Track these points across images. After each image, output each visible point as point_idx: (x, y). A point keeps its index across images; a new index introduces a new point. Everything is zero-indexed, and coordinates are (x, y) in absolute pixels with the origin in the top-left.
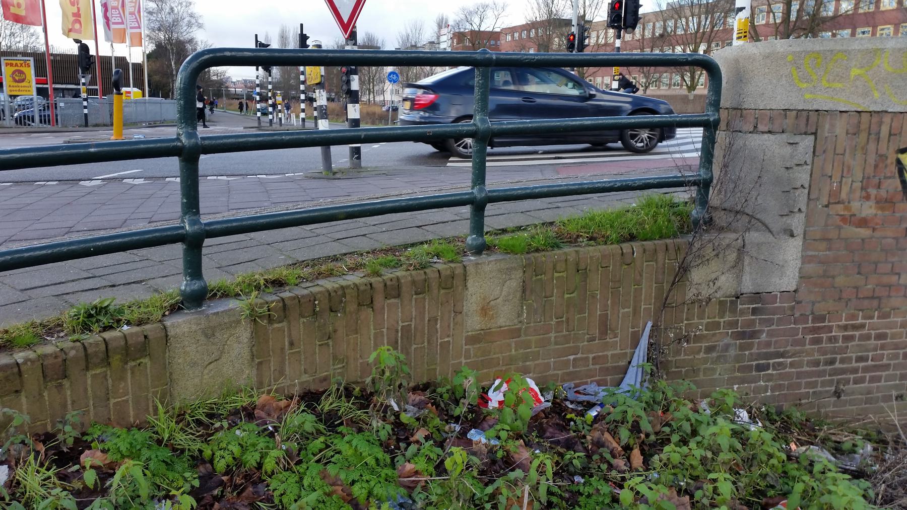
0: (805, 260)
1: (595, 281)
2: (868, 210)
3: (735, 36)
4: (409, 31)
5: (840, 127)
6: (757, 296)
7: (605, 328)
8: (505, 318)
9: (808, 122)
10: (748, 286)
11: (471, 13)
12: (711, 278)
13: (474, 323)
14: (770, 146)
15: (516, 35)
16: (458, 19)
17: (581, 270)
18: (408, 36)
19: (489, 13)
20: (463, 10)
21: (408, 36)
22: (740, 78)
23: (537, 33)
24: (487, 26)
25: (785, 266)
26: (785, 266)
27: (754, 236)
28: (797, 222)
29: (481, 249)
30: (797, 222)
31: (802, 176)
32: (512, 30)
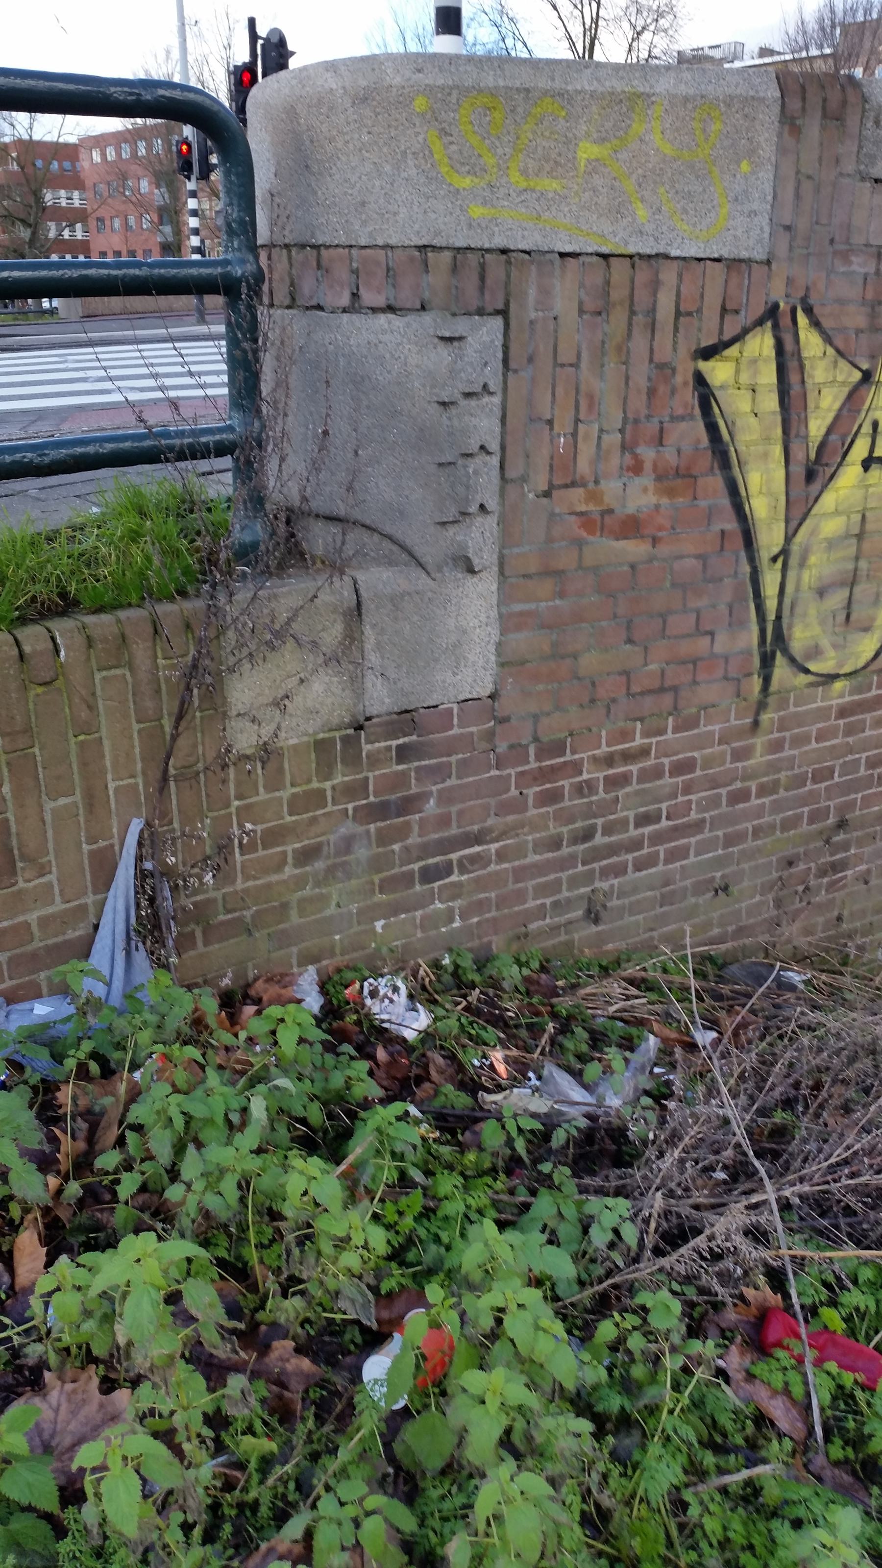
0: (508, 623)
2: (639, 496)
5: (565, 293)
6: (406, 719)
10: (380, 699)
14: (397, 347)
25: (462, 641)
26: (462, 641)
27: (377, 579)
30: (481, 538)
31: (483, 424)
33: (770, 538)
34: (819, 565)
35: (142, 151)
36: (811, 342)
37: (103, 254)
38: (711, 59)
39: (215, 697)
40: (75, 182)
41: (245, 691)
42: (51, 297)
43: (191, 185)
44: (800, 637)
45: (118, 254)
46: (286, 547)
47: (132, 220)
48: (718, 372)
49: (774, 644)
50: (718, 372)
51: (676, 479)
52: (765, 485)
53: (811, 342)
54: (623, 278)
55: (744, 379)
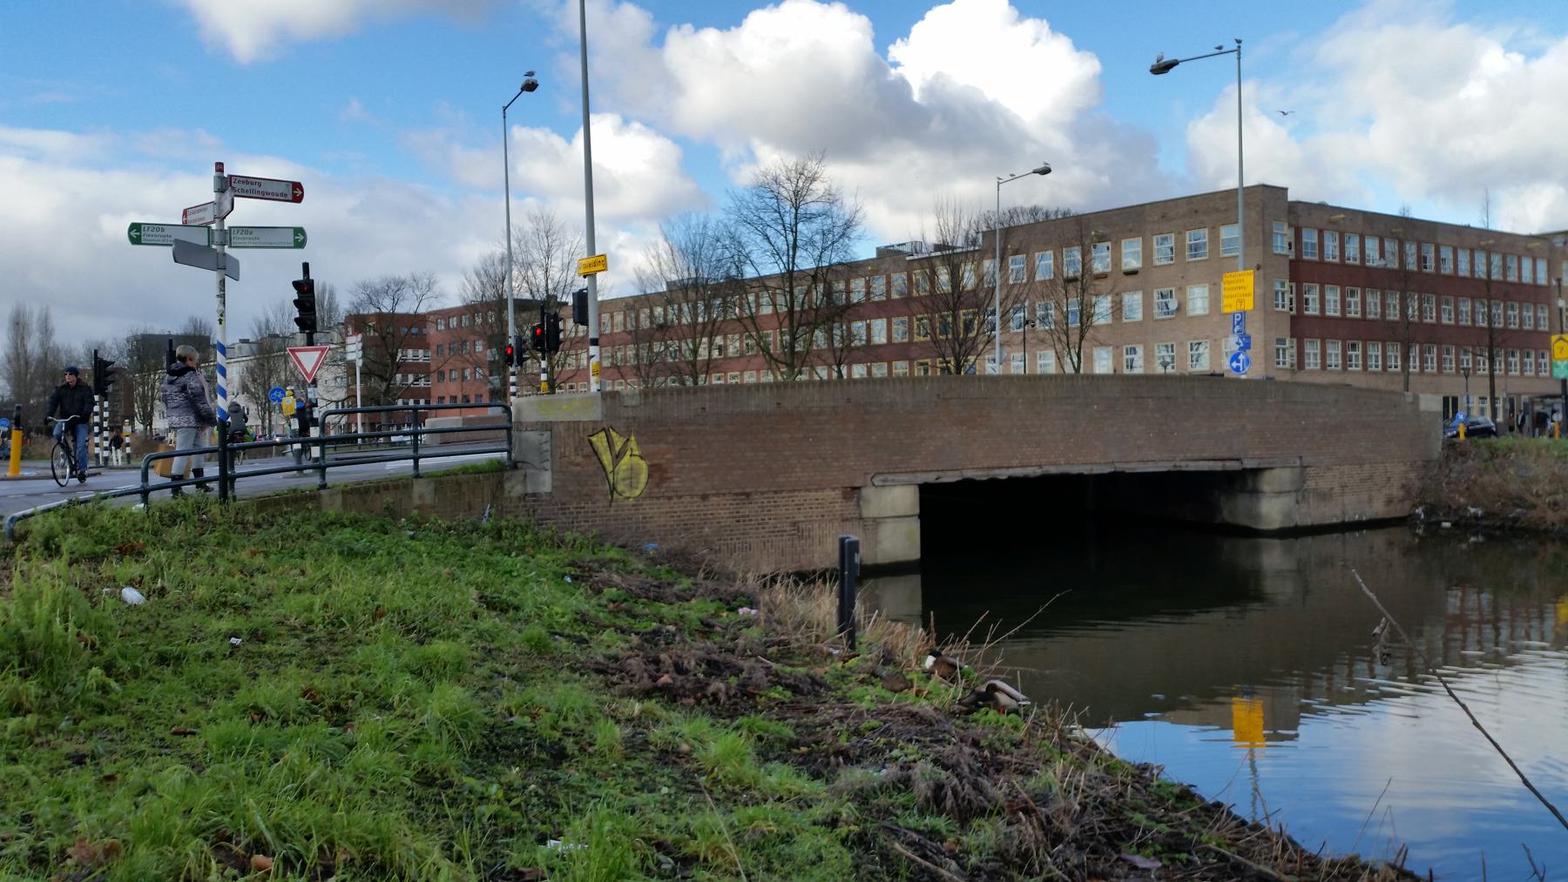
0: (554, 480)
1: (465, 488)
2: (579, 459)
3: (1241, 260)
4: (272, 318)
5: (561, 428)
6: (534, 495)
7: (470, 508)
8: (429, 500)
9: (547, 426)
10: (529, 490)
11: (377, 293)
12: (514, 488)
13: (417, 502)
14: (532, 436)
15: (454, 322)
16: (355, 300)
17: (459, 484)
18: (268, 321)
19: (407, 292)
20: (365, 287)
21: (268, 321)
22: (519, 411)
23: (485, 320)
24: (406, 307)
25: (545, 482)
26: (545, 482)
27: (529, 471)
28: (547, 465)
29: (418, 476)
30: (547, 465)
31: (547, 447)
32: (446, 314)
33: (609, 468)
34: (621, 475)
35: (479, 320)
36: (614, 434)
37: (441, 398)
38: (899, 252)
39: (502, 488)
40: (421, 342)
41: (507, 486)
42: (1032, 381)
43: (512, 369)
44: (620, 488)
45: (454, 398)
46: (515, 466)
47: (467, 373)
48: (594, 439)
49: (613, 489)
50: (594, 439)
51: (586, 456)
52: (607, 459)
53: (614, 434)
54: (573, 426)
55: (600, 441)
